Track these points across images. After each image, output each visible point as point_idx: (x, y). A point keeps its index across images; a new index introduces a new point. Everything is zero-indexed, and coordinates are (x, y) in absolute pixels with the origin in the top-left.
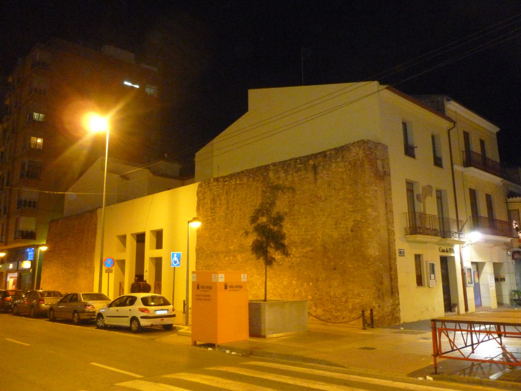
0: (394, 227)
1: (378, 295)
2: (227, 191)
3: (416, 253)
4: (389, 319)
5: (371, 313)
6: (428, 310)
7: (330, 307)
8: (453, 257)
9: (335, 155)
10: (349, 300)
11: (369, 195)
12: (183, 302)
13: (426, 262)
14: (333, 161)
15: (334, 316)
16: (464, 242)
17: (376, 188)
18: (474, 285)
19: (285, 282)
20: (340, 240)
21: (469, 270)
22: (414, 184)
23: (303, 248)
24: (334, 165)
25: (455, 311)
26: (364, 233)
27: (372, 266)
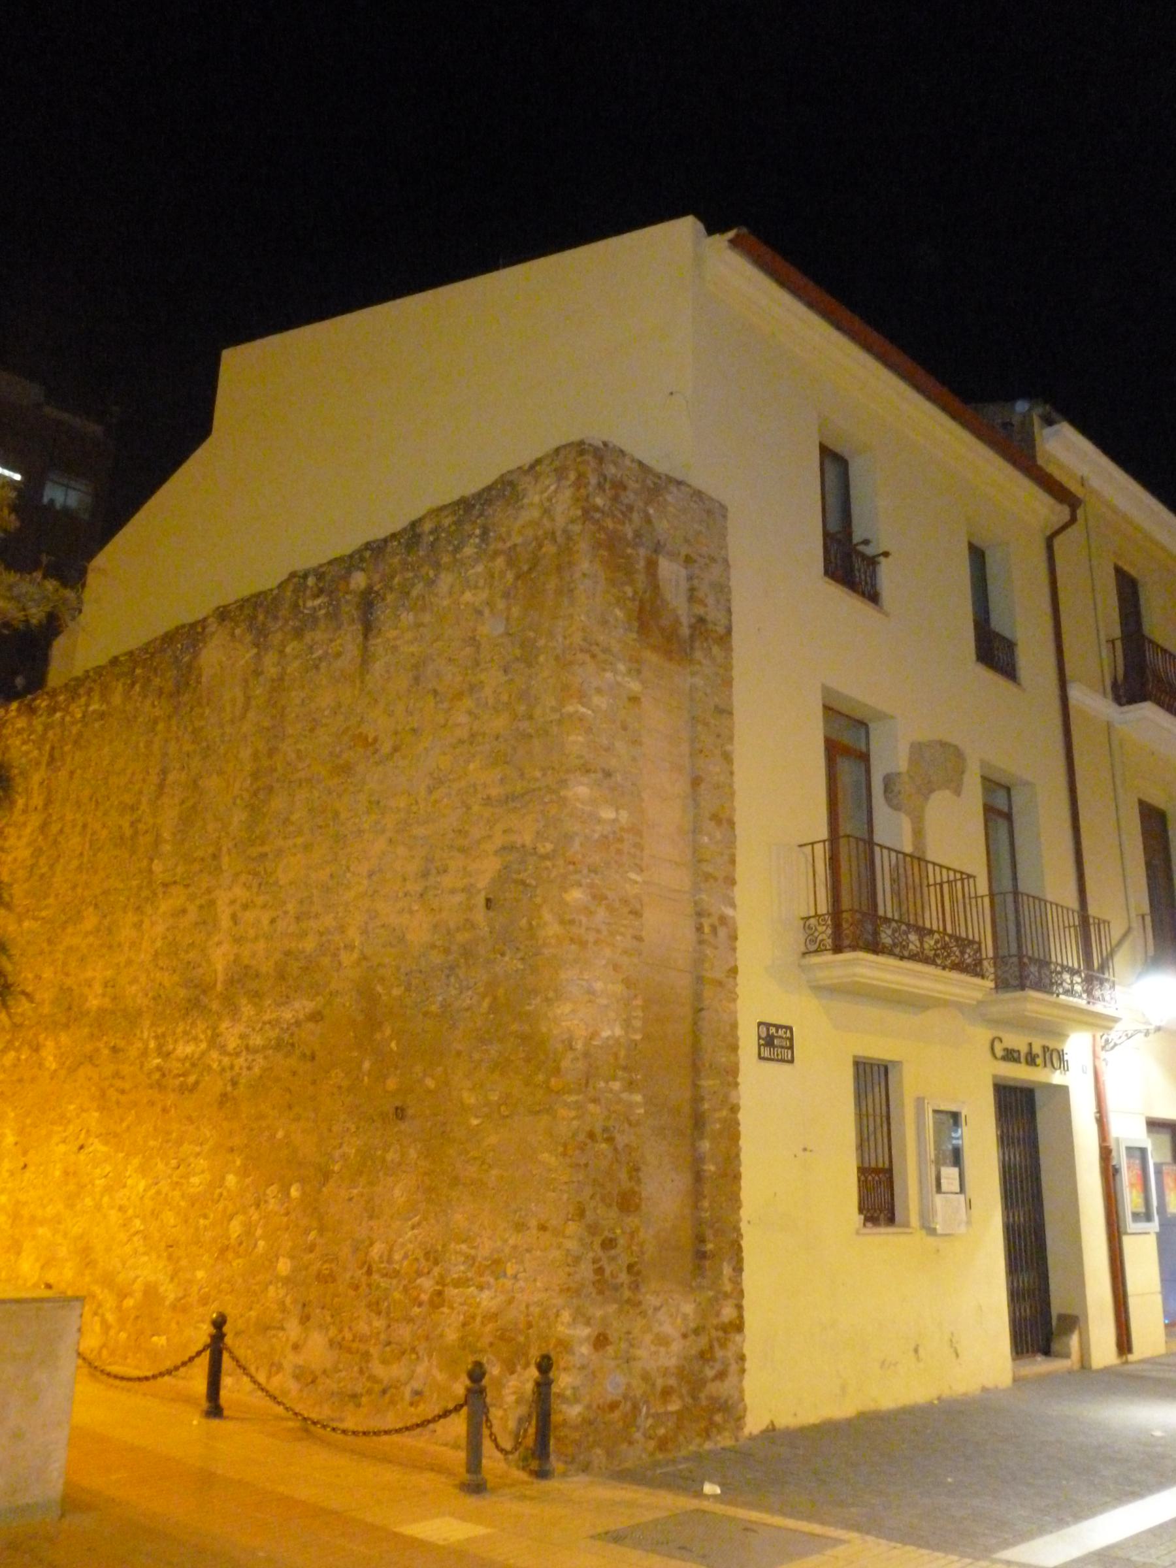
0: (733, 905)
1: (600, 1271)
2: (53, 748)
3: (861, 1053)
4: (667, 1413)
5: (544, 1386)
6: (921, 1351)
7: (362, 1327)
8: (1063, 1091)
9: (453, 528)
10: (451, 1292)
11: (583, 710)
13: (920, 1102)
14: (446, 559)
15: (373, 1379)
16: (1115, 1020)
17: (635, 686)
18: (1161, 1225)
19: (195, 1180)
20: (436, 958)
21: (1138, 1153)
22: (871, 726)
23: (286, 1001)
24: (446, 580)
25: (1067, 1356)
26: (547, 916)
27: (572, 1098)
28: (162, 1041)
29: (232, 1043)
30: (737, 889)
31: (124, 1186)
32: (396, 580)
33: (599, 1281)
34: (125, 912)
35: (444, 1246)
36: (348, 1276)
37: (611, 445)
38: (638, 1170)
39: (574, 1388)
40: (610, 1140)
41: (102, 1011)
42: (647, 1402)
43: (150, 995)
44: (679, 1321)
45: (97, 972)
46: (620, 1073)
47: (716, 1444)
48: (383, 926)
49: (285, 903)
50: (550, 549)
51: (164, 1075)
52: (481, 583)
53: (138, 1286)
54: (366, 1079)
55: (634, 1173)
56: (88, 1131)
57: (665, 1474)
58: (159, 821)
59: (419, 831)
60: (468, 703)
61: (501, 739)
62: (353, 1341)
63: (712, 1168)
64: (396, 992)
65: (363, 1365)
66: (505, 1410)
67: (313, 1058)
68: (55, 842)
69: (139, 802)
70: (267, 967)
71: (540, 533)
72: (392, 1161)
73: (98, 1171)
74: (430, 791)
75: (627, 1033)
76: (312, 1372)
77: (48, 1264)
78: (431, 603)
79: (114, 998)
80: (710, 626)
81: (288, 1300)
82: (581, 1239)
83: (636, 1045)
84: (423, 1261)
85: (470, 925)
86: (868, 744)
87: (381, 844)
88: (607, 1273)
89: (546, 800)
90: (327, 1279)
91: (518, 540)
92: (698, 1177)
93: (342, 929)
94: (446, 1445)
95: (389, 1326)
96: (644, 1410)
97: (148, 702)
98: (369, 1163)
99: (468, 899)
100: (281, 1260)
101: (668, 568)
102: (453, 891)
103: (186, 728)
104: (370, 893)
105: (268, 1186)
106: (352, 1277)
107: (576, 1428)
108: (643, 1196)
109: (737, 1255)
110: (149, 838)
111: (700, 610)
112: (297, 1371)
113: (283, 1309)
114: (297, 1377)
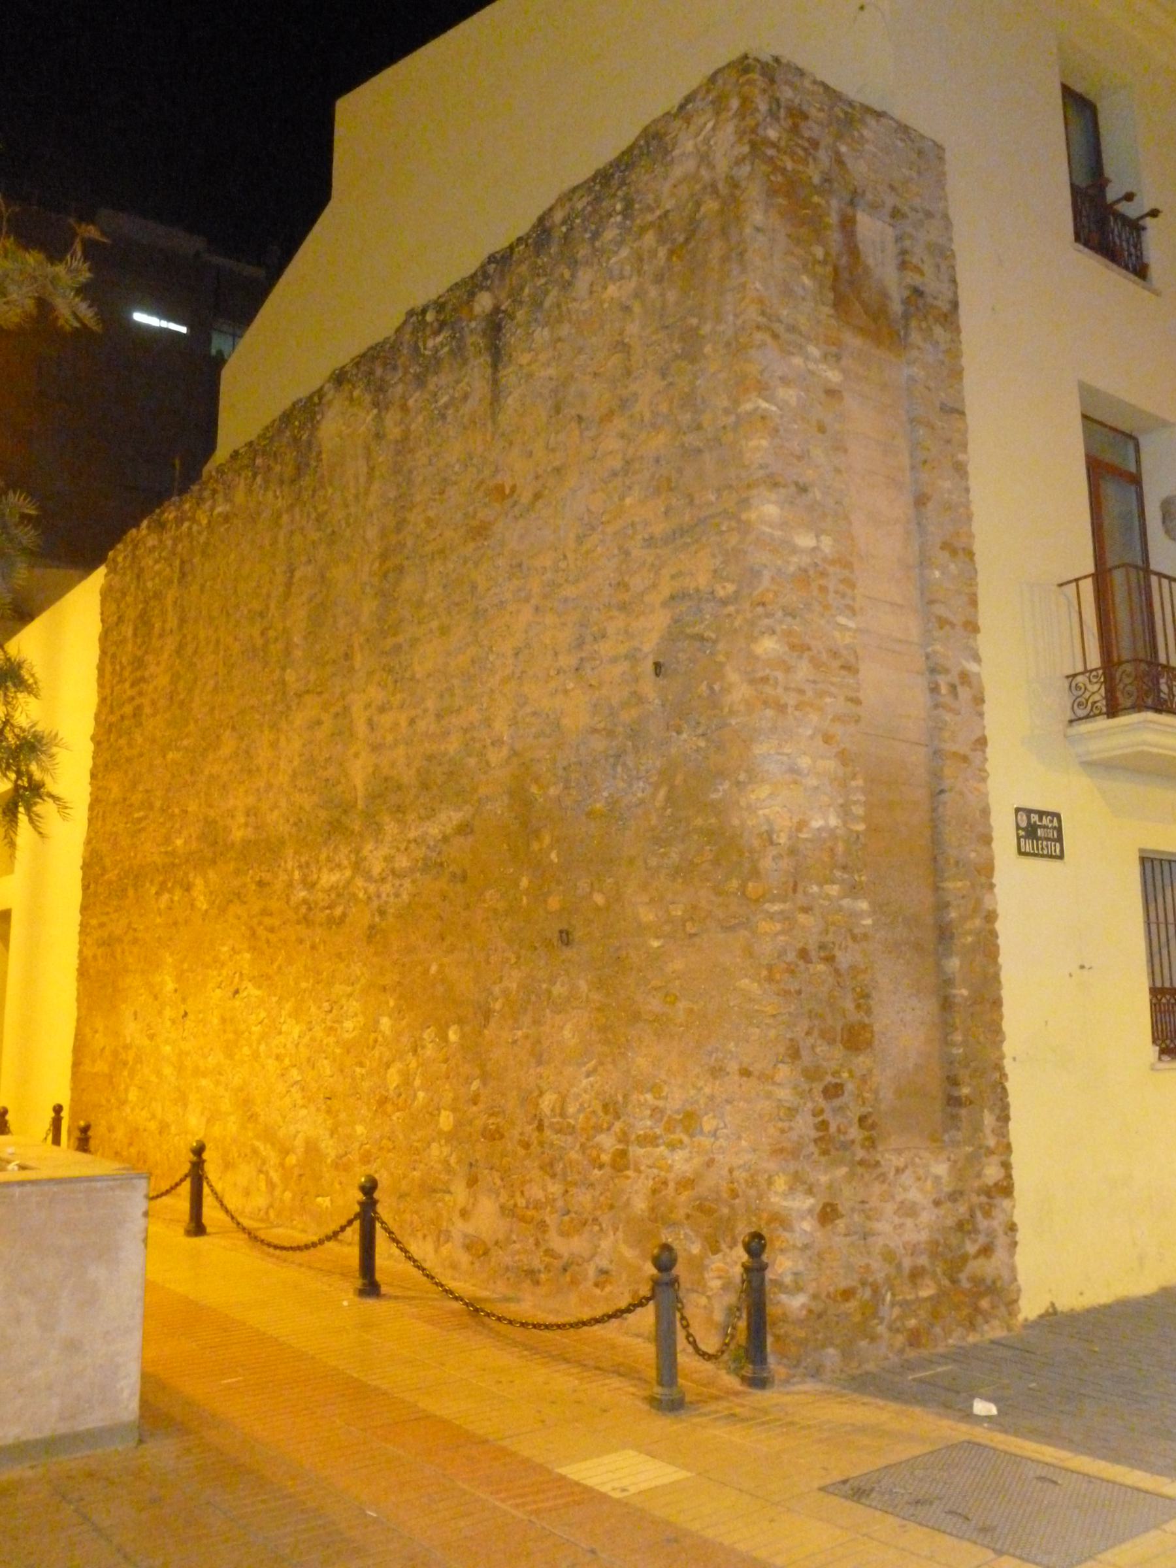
0: (977, 659)
1: (823, 1125)
2: (183, 562)
5: (755, 1271)
7: (536, 1193)
9: (589, 208)
10: (636, 1152)
11: (764, 405)
12: (52, 1114)
15: (549, 1252)
17: (834, 376)
19: (349, 1025)
20: (599, 744)
22: (1141, 440)
23: (431, 814)
24: (585, 276)
26: (733, 677)
27: (776, 907)
28: (306, 871)
29: (377, 868)
30: (979, 636)
31: (280, 1033)
32: (527, 291)
33: (821, 1139)
34: (262, 732)
35: (625, 1096)
36: (516, 1132)
37: (784, 61)
38: (867, 996)
39: (795, 1274)
40: (830, 959)
41: (246, 843)
42: (891, 1288)
43: (291, 821)
44: (929, 1184)
45: (239, 800)
46: (838, 874)
47: (982, 1336)
48: (534, 714)
49: (423, 700)
50: (711, 205)
51: (310, 909)
52: (627, 272)
53: (299, 1143)
54: (524, 898)
55: (862, 1001)
56: (241, 974)
57: (921, 1381)
58: (288, 624)
59: (570, 591)
60: (620, 423)
61: (663, 462)
62: (527, 1207)
63: (965, 992)
64: (553, 791)
65: (540, 1236)
66: (708, 1297)
67: (464, 878)
68: (192, 665)
69: (267, 607)
70: (408, 777)
71: (698, 187)
72: (559, 996)
73: (253, 1017)
74: (580, 540)
75: (845, 823)
76: (484, 1243)
77: (212, 1119)
78: (568, 310)
79: (257, 828)
80: (930, 300)
81: (453, 1160)
82: (795, 1087)
83: (858, 837)
84: (600, 1113)
85: (638, 699)
86: (1138, 462)
87: (527, 614)
88: (833, 1129)
89: (724, 528)
90: (494, 1135)
91: (669, 204)
92: (947, 1004)
93: (488, 722)
94: (638, 1335)
95: (567, 1191)
96: (889, 1297)
97: (270, 494)
98: (533, 998)
99: (632, 667)
100: (444, 1113)
101: (869, 227)
102: (614, 660)
103: (309, 515)
104: (518, 675)
105: (423, 1030)
106: (522, 1134)
107: (800, 1323)
108: (875, 1029)
109: (1001, 1100)
110: (280, 646)
111: (913, 279)
112: (468, 1241)
113: (448, 1169)
114: (468, 1248)
